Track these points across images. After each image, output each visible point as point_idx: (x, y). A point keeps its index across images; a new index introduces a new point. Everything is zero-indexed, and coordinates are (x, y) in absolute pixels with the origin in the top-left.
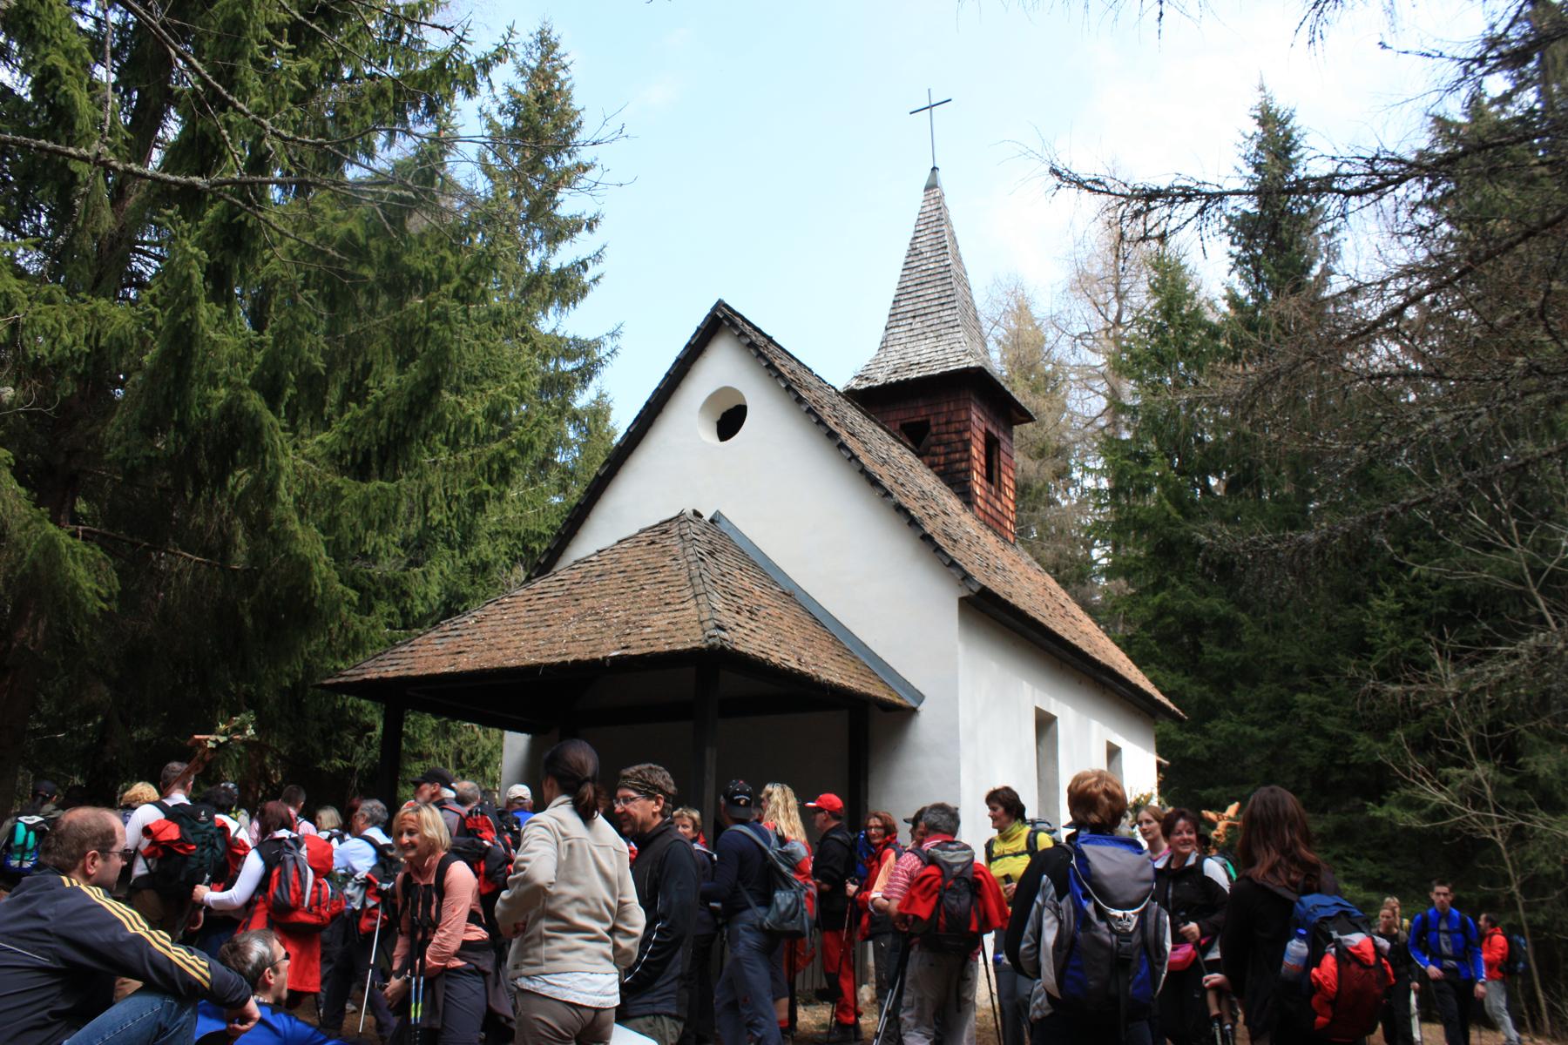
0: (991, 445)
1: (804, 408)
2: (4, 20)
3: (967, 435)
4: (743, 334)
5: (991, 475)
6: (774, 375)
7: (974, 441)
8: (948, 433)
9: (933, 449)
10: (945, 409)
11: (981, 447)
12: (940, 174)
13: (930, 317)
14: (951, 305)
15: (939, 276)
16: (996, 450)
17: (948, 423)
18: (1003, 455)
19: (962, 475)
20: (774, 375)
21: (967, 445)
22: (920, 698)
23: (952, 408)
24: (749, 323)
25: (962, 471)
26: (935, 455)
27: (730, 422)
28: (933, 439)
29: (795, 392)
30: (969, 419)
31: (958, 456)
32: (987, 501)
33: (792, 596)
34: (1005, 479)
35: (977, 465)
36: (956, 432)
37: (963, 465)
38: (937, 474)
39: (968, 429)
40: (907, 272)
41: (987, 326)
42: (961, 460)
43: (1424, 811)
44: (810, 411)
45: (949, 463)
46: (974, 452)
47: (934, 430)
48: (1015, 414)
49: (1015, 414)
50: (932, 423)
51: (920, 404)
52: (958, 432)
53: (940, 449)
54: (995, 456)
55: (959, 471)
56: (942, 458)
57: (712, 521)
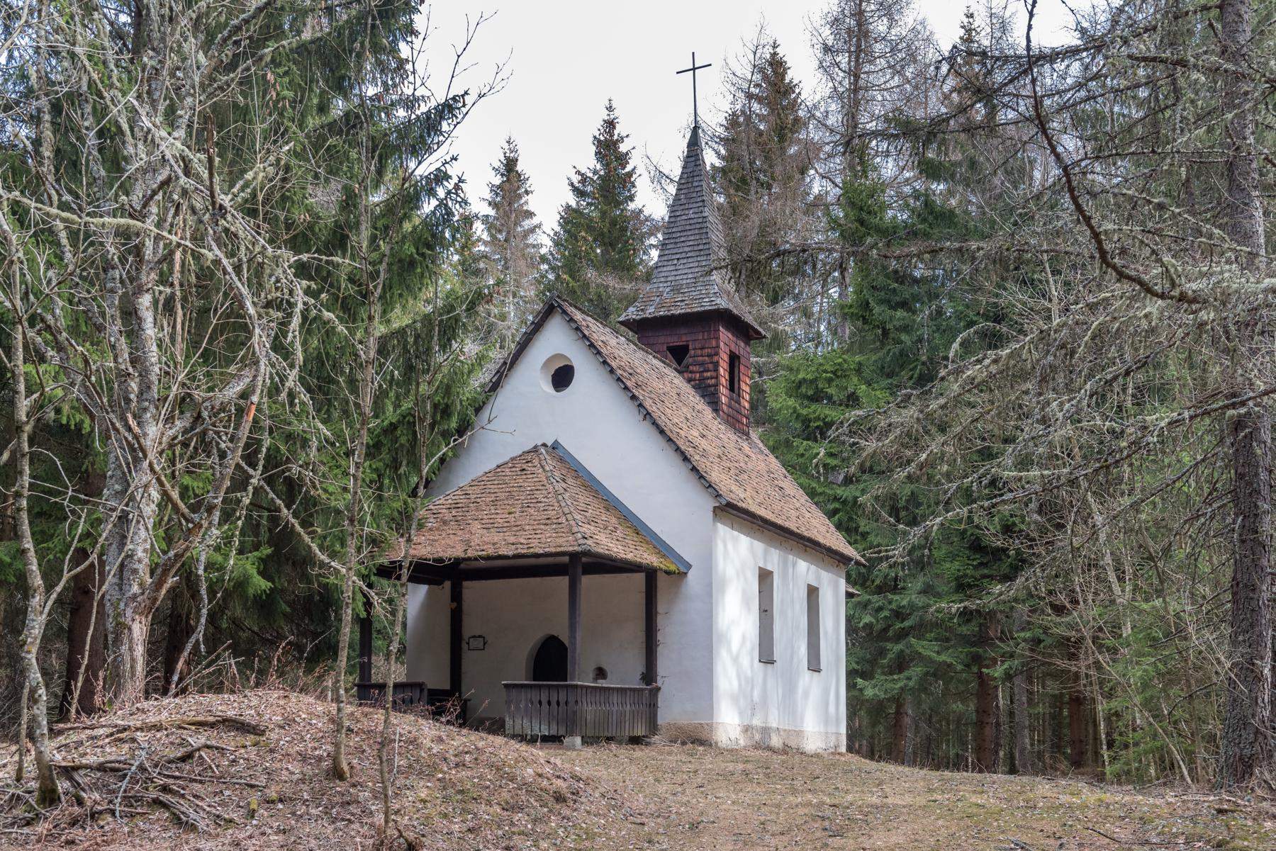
0: (734, 359)
1: (636, 404)
3: (715, 359)
7: (721, 362)
9: (691, 368)
13: (690, 260)
14: (707, 252)
15: (698, 226)
17: (702, 348)
22: (689, 566)
25: (713, 386)
27: (562, 377)
28: (691, 360)
30: (718, 347)
31: (709, 374)
32: (729, 406)
33: (612, 504)
34: (743, 386)
35: (723, 381)
38: (693, 387)
39: (717, 354)
46: (721, 371)
47: (692, 352)
50: (690, 347)
52: (709, 356)
55: (710, 386)
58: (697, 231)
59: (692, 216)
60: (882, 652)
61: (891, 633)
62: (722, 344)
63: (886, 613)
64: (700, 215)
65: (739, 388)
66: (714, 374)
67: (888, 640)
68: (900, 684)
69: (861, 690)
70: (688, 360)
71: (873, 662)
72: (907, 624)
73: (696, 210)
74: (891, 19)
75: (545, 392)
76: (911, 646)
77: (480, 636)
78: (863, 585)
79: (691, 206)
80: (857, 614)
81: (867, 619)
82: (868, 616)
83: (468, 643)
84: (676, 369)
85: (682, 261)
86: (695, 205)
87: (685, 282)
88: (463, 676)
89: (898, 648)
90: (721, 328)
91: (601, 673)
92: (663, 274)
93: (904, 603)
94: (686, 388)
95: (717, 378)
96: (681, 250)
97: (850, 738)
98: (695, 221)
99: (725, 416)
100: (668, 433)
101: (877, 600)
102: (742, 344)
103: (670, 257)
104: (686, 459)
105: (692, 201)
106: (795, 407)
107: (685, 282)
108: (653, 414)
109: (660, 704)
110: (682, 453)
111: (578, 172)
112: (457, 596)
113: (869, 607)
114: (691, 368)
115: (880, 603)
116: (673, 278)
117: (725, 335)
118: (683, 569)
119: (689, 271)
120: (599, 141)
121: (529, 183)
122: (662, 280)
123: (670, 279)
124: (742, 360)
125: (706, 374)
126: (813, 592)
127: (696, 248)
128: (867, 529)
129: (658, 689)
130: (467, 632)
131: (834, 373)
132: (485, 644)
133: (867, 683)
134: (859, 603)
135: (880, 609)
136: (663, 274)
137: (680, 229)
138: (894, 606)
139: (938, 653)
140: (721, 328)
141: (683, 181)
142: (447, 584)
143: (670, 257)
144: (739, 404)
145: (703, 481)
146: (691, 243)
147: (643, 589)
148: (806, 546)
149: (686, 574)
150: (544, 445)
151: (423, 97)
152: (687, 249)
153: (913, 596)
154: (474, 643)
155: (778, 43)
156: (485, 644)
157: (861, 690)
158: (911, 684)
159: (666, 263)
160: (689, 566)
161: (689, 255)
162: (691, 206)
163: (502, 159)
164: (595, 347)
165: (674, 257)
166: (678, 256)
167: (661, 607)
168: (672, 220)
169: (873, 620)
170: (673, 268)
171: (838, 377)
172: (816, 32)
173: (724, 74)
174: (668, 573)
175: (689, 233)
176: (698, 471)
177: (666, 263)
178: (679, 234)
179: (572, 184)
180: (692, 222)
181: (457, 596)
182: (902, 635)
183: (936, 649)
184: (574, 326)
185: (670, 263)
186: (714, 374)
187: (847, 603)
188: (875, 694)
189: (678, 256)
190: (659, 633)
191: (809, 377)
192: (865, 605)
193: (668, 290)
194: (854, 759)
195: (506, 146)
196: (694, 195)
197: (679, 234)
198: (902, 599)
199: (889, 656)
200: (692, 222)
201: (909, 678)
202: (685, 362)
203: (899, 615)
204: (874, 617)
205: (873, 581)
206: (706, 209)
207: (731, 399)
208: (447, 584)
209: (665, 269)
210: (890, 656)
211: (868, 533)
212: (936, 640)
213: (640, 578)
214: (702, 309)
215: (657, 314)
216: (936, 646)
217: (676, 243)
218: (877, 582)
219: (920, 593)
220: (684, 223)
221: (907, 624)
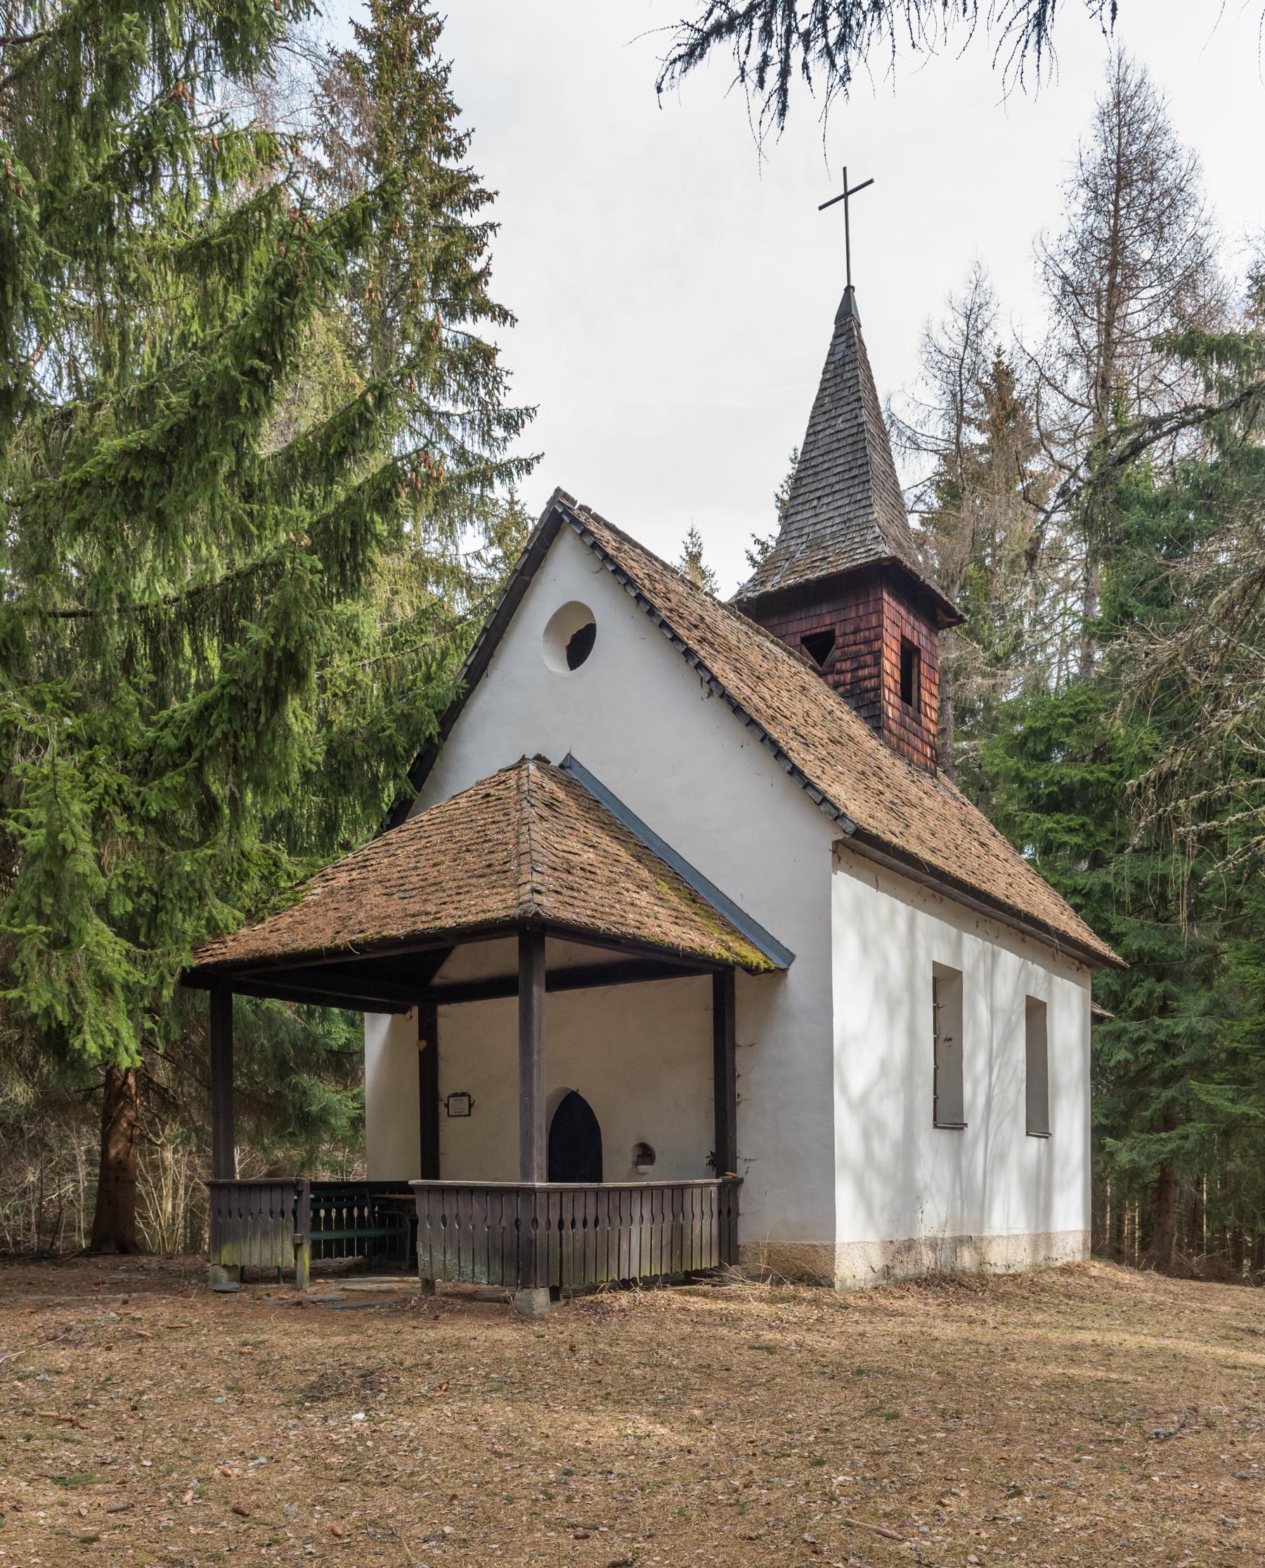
0: (909, 653)
2: (1262, 862)
3: (877, 645)
4: (586, 532)
5: (907, 692)
6: (623, 581)
7: (886, 651)
8: (855, 644)
9: (838, 665)
10: (853, 615)
11: (894, 658)
12: (858, 296)
13: (838, 496)
14: (864, 478)
16: (915, 661)
17: (856, 632)
18: (924, 667)
19: (872, 694)
20: (623, 581)
21: (878, 656)
22: (790, 957)
23: (861, 613)
24: (597, 519)
25: (871, 677)
26: (840, 672)
28: (838, 653)
29: (646, 601)
30: (881, 626)
31: (866, 672)
32: (902, 725)
34: (926, 697)
35: (889, 682)
36: (865, 643)
37: (873, 682)
38: (842, 695)
39: (879, 637)
40: (812, 439)
41: (909, 499)
42: (871, 677)
43: (55, 869)
44: (663, 625)
45: (856, 682)
46: (887, 666)
47: (840, 641)
48: (942, 616)
49: (942, 616)
50: (837, 633)
51: (824, 611)
52: (867, 642)
53: (846, 665)
54: (915, 671)
55: (867, 691)
56: (849, 676)
57: (562, 766)
58: (848, 449)
59: (842, 426)
60: (1143, 1100)
61: (1156, 1075)
62: (887, 623)
63: (1150, 1046)
64: (854, 422)
65: (919, 699)
66: (873, 670)
67: (1152, 1083)
68: (1169, 1147)
69: (1111, 1154)
70: (835, 653)
71: (1127, 1115)
72: (1180, 1061)
73: (848, 416)
74: (1161, 239)
75: (551, 673)
76: (1190, 1091)
77: (463, 1094)
78: (1114, 1009)
79: (839, 411)
80: (1106, 1049)
81: (1121, 1055)
82: (1123, 1050)
83: (447, 1106)
84: (812, 668)
85: (825, 500)
86: (846, 409)
87: (828, 531)
88: (442, 1159)
89: (1167, 1094)
90: (885, 596)
91: (645, 1154)
92: (796, 525)
93: (1180, 1029)
94: (832, 701)
95: (879, 676)
96: (824, 483)
97: (1096, 1228)
98: (846, 433)
99: (894, 740)
100: (750, 711)
101: (1136, 1028)
102: (924, 630)
103: (807, 497)
104: (780, 754)
105: (842, 403)
106: (1018, 769)
107: (828, 531)
108: (721, 679)
109: (742, 1207)
110: (774, 743)
111: (757, 541)
112: (428, 1031)
113: (1125, 1038)
114: (838, 665)
115: (1141, 1033)
116: (811, 529)
117: (891, 608)
118: (776, 962)
119: (836, 513)
120: (782, 501)
121: (714, 579)
122: (795, 534)
123: (806, 531)
124: (924, 655)
125: (861, 673)
126: (1036, 1011)
127: (846, 476)
128: (1122, 929)
129: (738, 1183)
130: (445, 1089)
131: (1074, 716)
132: (470, 1105)
133: (1120, 1144)
134: (1110, 1033)
135: (1141, 1040)
136: (796, 525)
137: (822, 451)
138: (1162, 1036)
139: (1233, 1101)
140: (885, 596)
141: (828, 376)
142: (415, 1011)
143: (807, 497)
144: (919, 723)
145: (811, 792)
146: (840, 469)
147: (710, 1002)
148: (1023, 932)
149: (784, 971)
150: (540, 760)
151: (527, 409)
152: (834, 480)
153: (1194, 1020)
154: (461, 1105)
155: (1003, 349)
156: (470, 1105)
157: (1111, 1154)
158: (1188, 1145)
159: (800, 508)
160: (790, 957)
161: (837, 487)
162: (839, 411)
163: (684, 554)
164: (624, 574)
165: (812, 496)
166: (819, 494)
167: (742, 1035)
168: (812, 439)
169: (1130, 1057)
170: (811, 513)
171: (1080, 722)
172: (1050, 262)
173: (925, 356)
174: (752, 970)
175: (836, 454)
176: (801, 773)
177: (800, 508)
178: (820, 460)
179: (751, 558)
180: (840, 435)
181: (428, 1031)
182: (1168, 1079)
183: (1230, 1095)
184: (589, 541)
185: (807, 506)
186: (873, 670)
187: (1093, 1033)
188: (1133, 1160)
189: (819, 494)
190: (738, 1082)
191: (1039, 724)
192: (1118, 1036)
193: (804, 547)
194: (1098, 1268)
195: (688, 540)
196: (846, 393)
197: (820, 460)
198: (1176, 1024)
199: (1153, 1106)
200: (840, 435)
201: (1185, 1137)
202: (829, 658)
203: (1167, 1047)
204: (1131, 1051)
205: (1130, 1003)
206: (863, 411)
207: (904, 713)
208: (415, 1011)
209: (799, 517)
210: (1156, 1105)
211: (1124, 935)
212: (1228, 1081)
213: (705, 982)
214: (854, 564)
215: (783, 584)
216: (1230, 1090)
217: (816, 474)
218: (1138, 1003)
219: (1204, 1015)
220: (828, 440)
221: (1180, 1061)
